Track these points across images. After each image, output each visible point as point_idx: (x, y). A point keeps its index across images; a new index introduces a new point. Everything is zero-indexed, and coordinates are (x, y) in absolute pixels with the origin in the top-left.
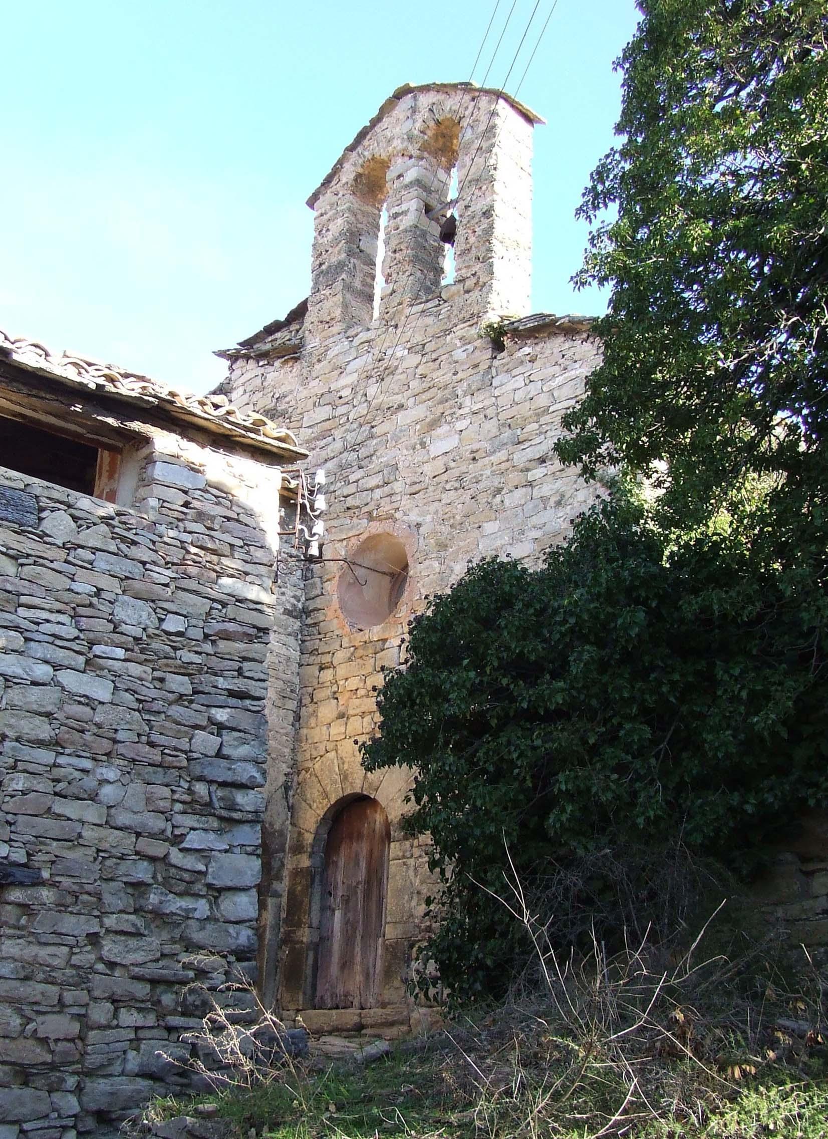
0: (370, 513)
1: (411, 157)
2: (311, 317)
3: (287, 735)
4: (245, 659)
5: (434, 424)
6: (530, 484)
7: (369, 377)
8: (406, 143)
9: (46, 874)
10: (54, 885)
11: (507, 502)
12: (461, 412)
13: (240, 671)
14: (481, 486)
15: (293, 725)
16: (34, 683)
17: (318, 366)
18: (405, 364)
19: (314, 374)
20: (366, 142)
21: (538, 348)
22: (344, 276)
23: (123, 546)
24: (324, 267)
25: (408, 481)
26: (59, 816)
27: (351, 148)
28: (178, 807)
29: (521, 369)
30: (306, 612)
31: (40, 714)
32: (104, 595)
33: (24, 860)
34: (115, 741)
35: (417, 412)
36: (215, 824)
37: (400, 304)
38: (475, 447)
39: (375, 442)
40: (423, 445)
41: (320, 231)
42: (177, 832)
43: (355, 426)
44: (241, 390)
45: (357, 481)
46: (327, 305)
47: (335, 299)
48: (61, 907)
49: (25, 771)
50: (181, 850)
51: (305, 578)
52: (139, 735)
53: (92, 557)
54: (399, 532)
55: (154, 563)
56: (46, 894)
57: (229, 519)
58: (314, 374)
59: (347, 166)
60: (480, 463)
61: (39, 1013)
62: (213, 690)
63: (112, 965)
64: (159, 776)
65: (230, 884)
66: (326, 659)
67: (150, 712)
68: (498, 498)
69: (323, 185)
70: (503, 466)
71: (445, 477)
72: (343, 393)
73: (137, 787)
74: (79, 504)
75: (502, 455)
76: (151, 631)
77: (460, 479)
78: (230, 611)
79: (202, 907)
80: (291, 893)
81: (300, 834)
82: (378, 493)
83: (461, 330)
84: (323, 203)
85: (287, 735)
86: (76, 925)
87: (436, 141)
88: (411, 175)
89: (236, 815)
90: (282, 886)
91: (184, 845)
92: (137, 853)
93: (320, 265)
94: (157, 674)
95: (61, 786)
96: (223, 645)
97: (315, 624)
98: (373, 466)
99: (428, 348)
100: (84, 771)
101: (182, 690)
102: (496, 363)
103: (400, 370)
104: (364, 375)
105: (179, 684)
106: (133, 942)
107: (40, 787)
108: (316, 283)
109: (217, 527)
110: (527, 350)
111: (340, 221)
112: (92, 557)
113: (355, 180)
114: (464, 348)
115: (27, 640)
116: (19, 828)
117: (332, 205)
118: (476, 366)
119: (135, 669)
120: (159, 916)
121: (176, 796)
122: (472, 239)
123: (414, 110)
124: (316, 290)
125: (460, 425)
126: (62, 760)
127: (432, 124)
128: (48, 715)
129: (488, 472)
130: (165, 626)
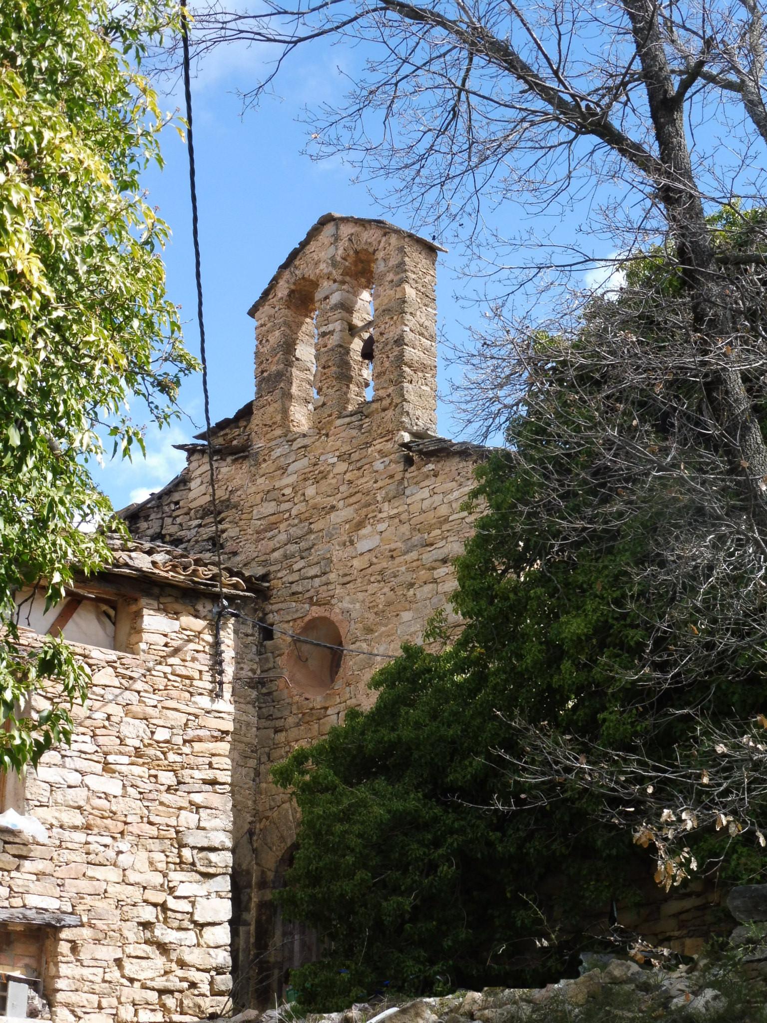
0: (311, 598)
1: (335, 281)
2: (257, 419)
3: (249, 789)
4: (213, 755)
5: (360, 525)
6: (435, 581)
7: (305, 479)
8: (330, 269)
9: (85, 919)
10: (91, 926)
11: (418, 595)
12: (381, 515)
13: (210, 765)
14: (399, 579)
15: (254, 780)
16: (70, 787)
17: (264, 465)
18: (336, 471)
19: (261, 472)
20: (297, 262)
21: (439, 465)
22: (282, 385)
23: (123, 681)
24: (265, 374)
25: (341, 573)
26: (92, 878)
27: (284, 267)
28: (172, 866)
29: (427, 483)
30: (261, 682)
31: (75, 808)
32: (112, 718)
33: (70, 910)
34: (126, 823)
35: (344, 513)
36: (198, 877)
37: (330, 416)
38: (393, 546)
39: (313, 537)
40: (352, 543)
41: (261, 339)
42: (171, 885)
43: (296, 521)
44: (198, 481)
45: (299, 570)
46: (270, 409)
47: (275, 405)
48: (97, 941)
49: (67, 848)
50: (175, 897)
51: (259, 653)
52: (142, 817)
53: (102, 692)
54: (335, 615)
55: (146, 691)
56: (86, 932)
57: (198, 651)
58: (261, 472)
59: (282, 282)
60: (397, 560)
61: (85, 1013)
62: (191, 781)
63: (132, 980)
64: (155, 845)
65: (210, 920)
66: (279, 723)
67: (148, 800)
68: (411, 592)
69: (261, 298)
70: (415, 564)
71: (369, 571)
72: (287, 491)
73: (143, 855)
74: (93, 654)
75: (414, 555)
76: (146, 741)
77: (381, 573)
78: (201, 721)
79: (190, 937)
80: (258, 922)
81: (263, 872)
82: (317, 581)
83: (379, 445)
84: (266, 310)
85: (249, 789)
86: (108, 953)
87: (356, 266)
88: (335, 298)
89: (212, 870)
90: (251, 916)
91: (176, 894)
92: (145, 901)
93: (262, 372)
94: (153, 772)
95: (92, 857)
96: (197, 746)
97: (269, 694)
98: (313, 558)
99: (355, 457)
100: (105, 846)
101: (169, 783)
102: (408, 475)
103: (331, 475)
104: (301, 478)
105: (167, 778)
106: (144, 963)
107: (78, 859)
108: (259, 385)
109: (189, 659)
110: (431, 466)
111: (277, 333)
112: (102, 692)
113: (289, 295)
114: (382, 462)
115: (63, 756)
116: (67, 888)
117: (270, 317)
118: (392, 477)
119: (137, 770)
120: (163, 948)
121: (170, 860)
122: (387, 364)
123: (337, 238)
124: (259, 395)
125: (381, 527)
126: (91, 839)
127: (351, 253)
128: (79, 808)
129: (403, 569)
130: (156, 737)
